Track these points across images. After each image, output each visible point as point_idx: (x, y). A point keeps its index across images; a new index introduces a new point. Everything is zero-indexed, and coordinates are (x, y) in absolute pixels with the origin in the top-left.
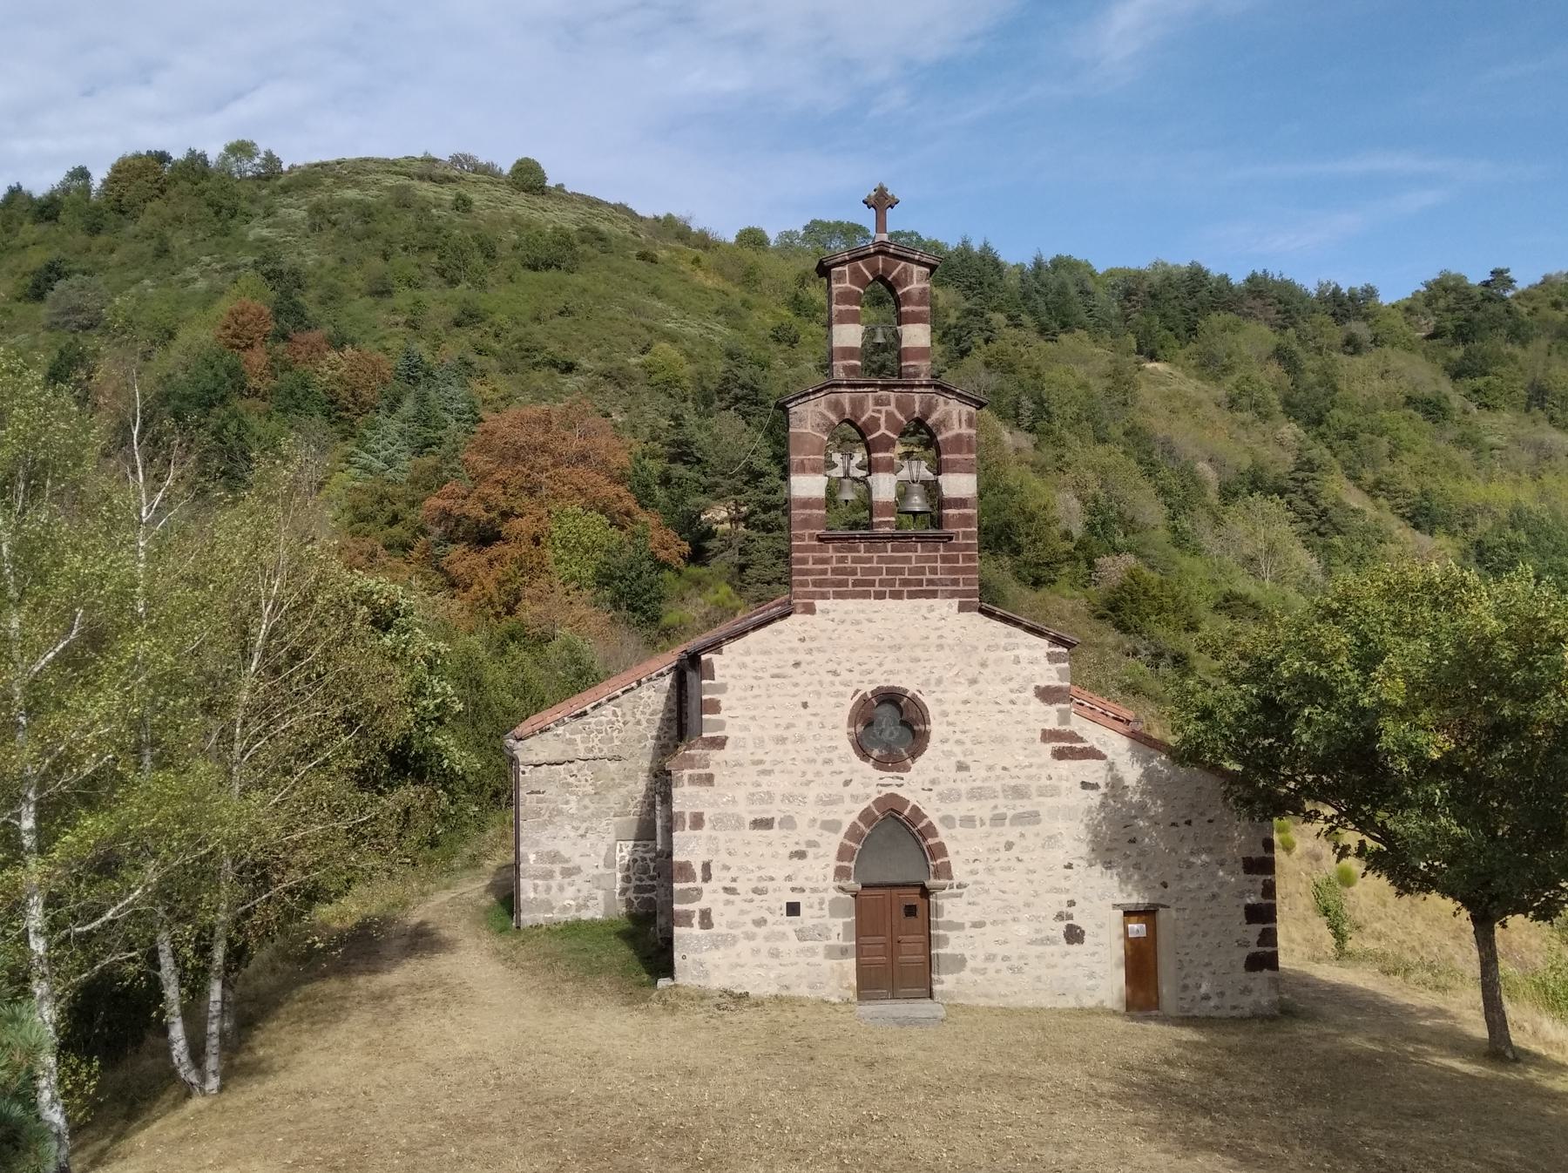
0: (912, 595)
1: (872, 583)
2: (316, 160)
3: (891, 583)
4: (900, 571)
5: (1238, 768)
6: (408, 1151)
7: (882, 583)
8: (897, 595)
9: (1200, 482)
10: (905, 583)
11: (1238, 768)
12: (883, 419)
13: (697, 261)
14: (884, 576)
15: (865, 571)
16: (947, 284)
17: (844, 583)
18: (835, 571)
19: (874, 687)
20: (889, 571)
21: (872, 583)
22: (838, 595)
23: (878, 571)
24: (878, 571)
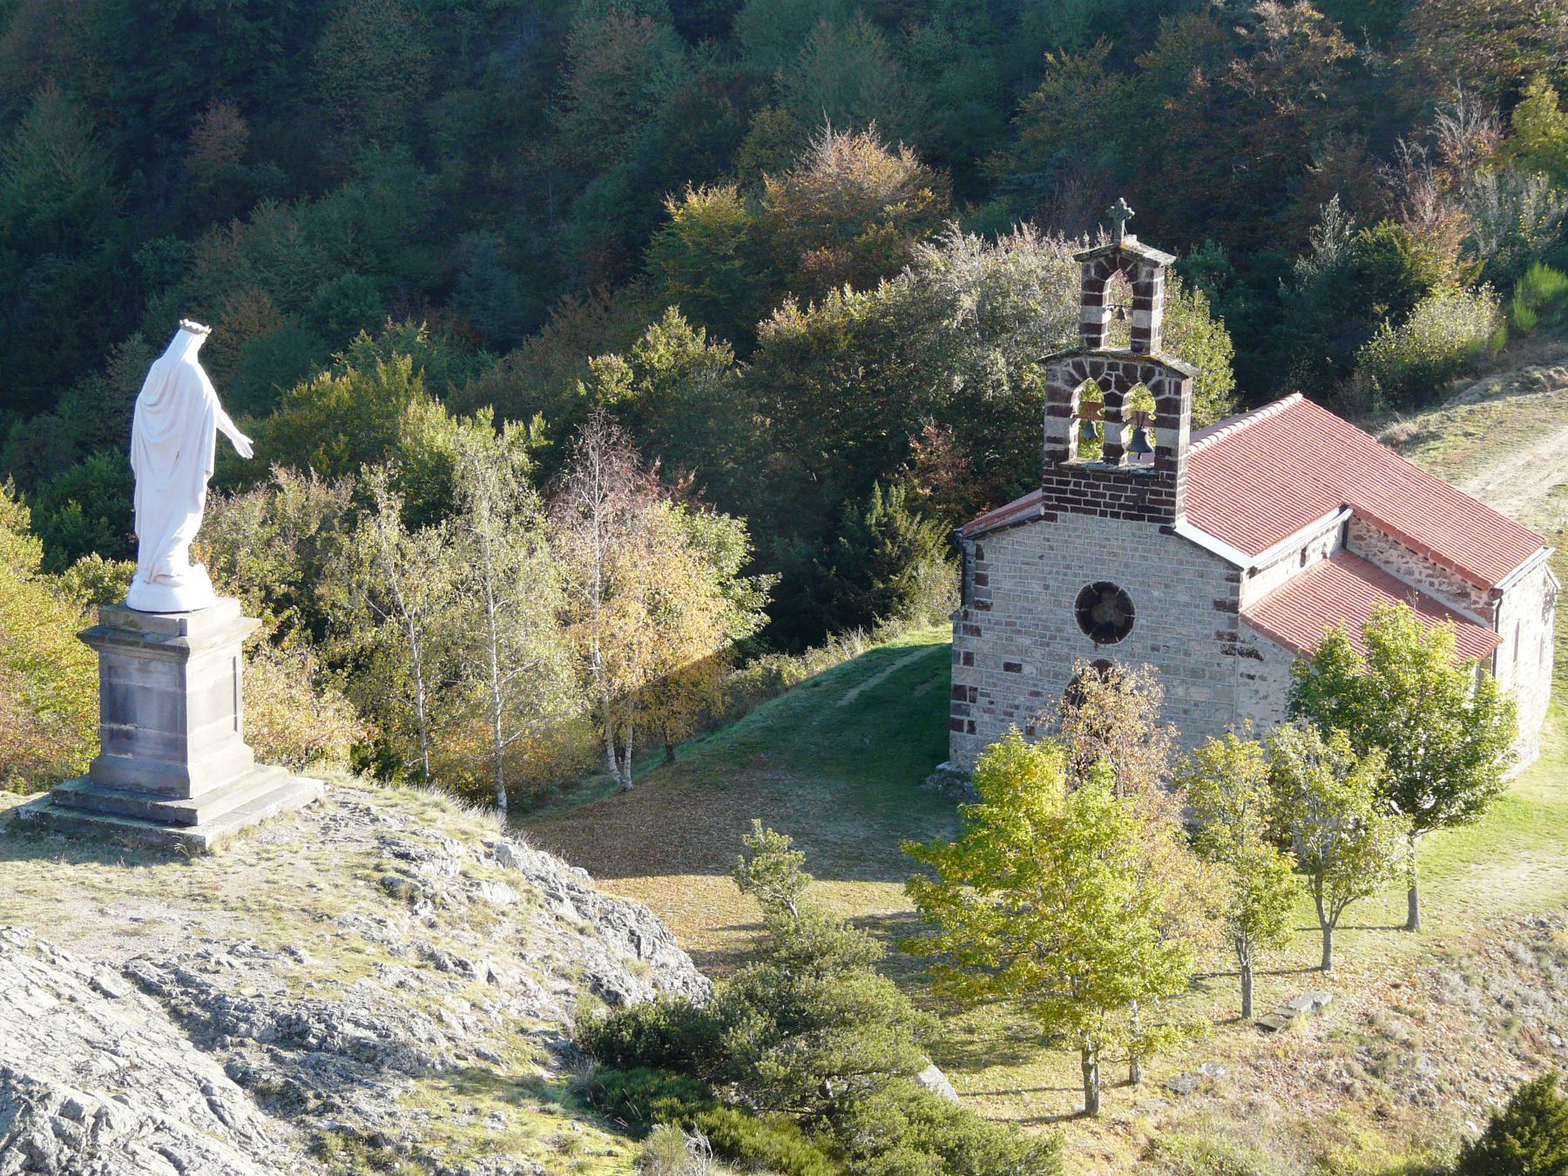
0: (1127, 517)
1: (1098, 504)
2: (137, 478)
3: (1113, 506)
4: (1119, 498)
5: (1238, 29)
6: (1058, 168)
7: (1106, 505)
8: (1115, 515)
9: (1391, 324)
10: (1121, 506)
11: (1238, 29)
12: (1113, 380)
13: (475, 1111)
14: (1107, 500)
15: (1094, 495)
16: (1207, 761)
17: (1079, 502)
18: (1072, 492)
19: (1095, 581)
20: (1112, 497)
21: (1098, 504)
22: (1073, 510)
23: (1104, 496)
24: (1104, 496)
